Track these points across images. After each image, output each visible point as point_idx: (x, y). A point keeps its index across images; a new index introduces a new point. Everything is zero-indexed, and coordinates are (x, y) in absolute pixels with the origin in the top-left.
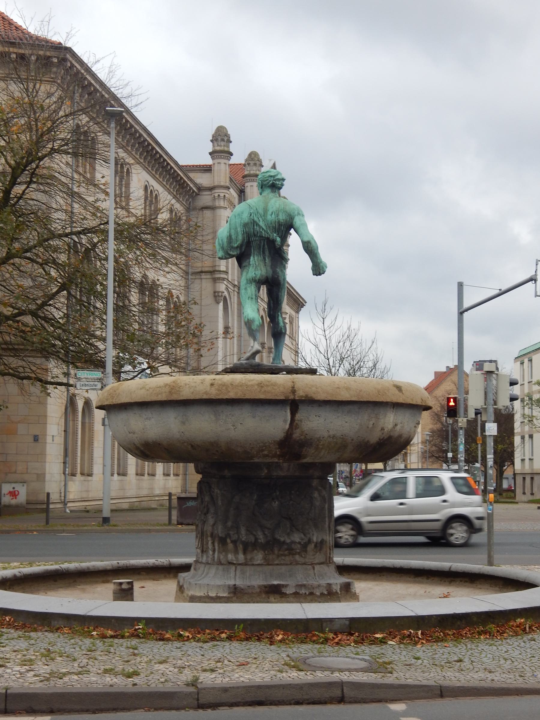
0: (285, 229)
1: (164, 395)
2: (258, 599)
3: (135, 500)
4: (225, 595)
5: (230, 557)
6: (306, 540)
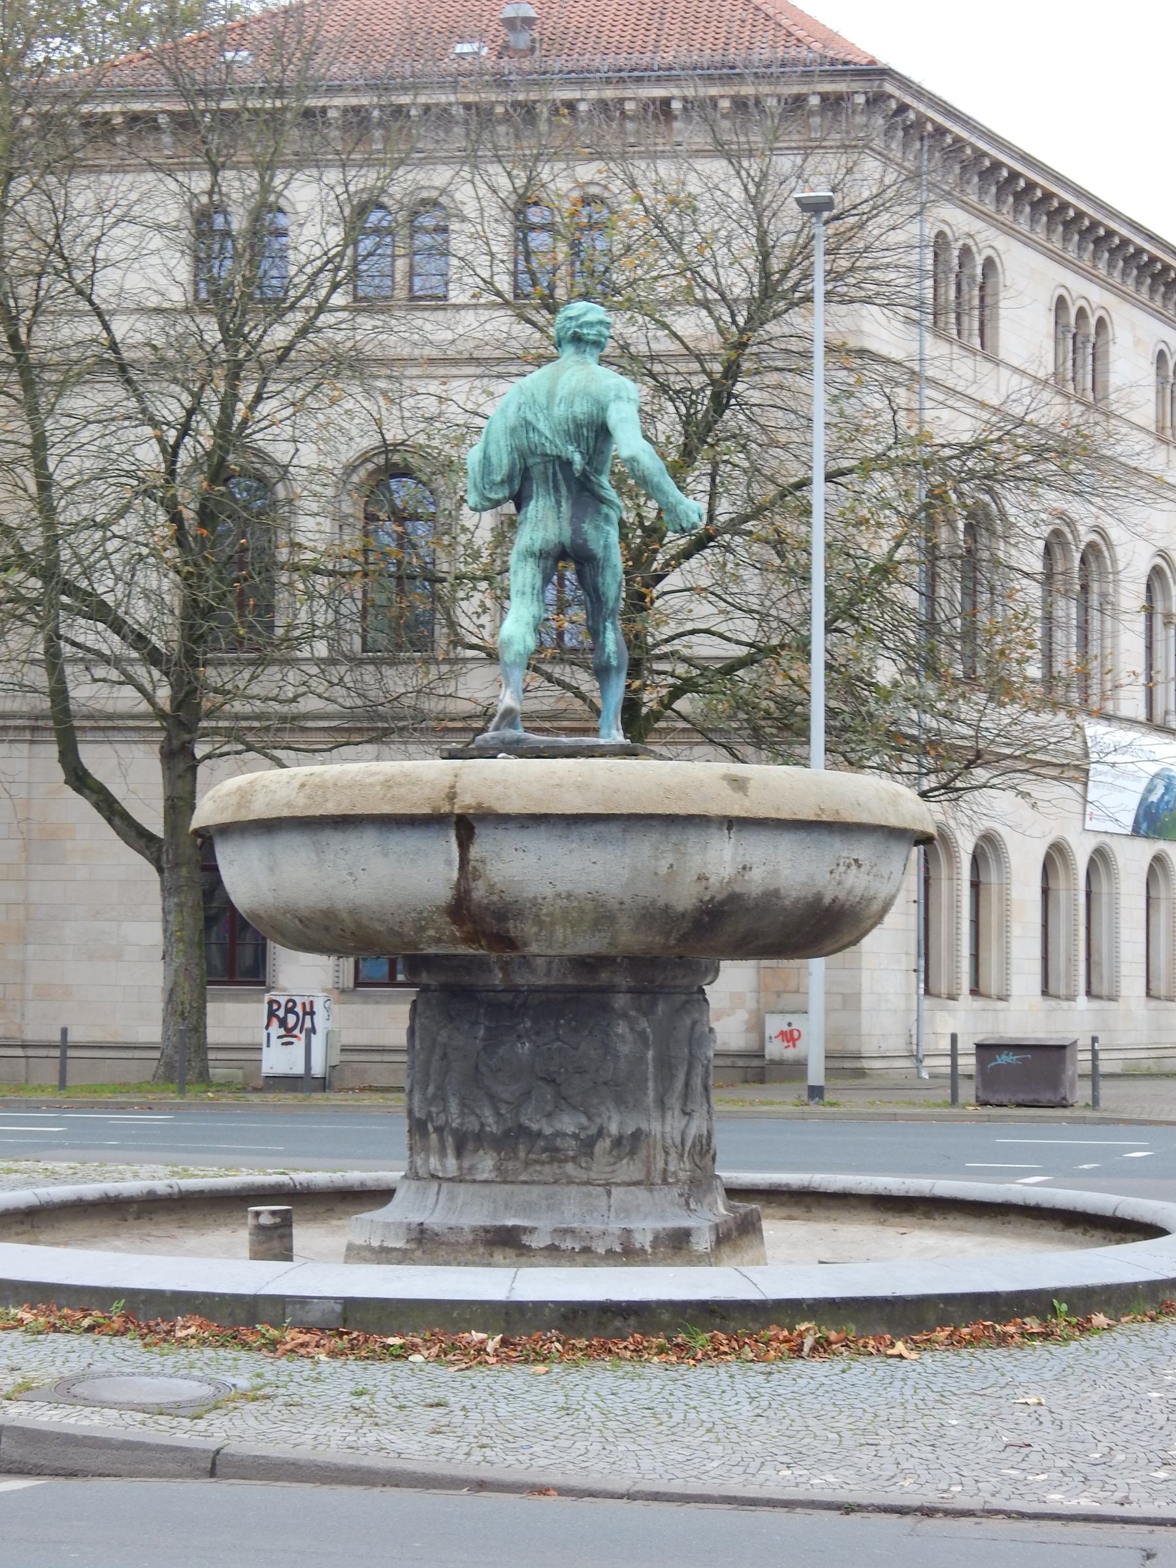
0: (592, 435)
1: (230, 811)
2: (469, 1256)
3: (1143, 1054)
4: (401, 1244)
5: (434, 1162)
6: (593, 1130)
